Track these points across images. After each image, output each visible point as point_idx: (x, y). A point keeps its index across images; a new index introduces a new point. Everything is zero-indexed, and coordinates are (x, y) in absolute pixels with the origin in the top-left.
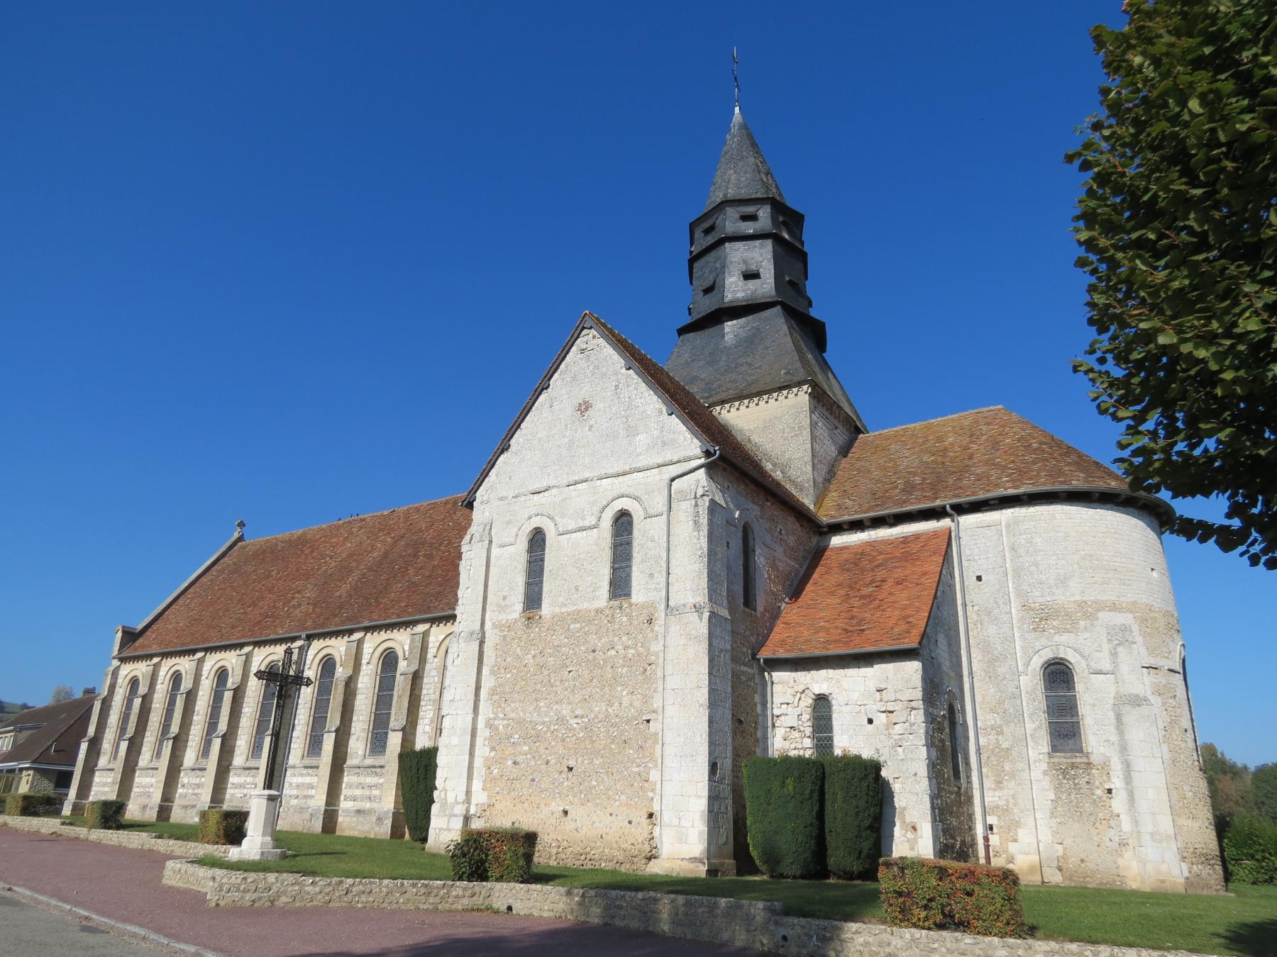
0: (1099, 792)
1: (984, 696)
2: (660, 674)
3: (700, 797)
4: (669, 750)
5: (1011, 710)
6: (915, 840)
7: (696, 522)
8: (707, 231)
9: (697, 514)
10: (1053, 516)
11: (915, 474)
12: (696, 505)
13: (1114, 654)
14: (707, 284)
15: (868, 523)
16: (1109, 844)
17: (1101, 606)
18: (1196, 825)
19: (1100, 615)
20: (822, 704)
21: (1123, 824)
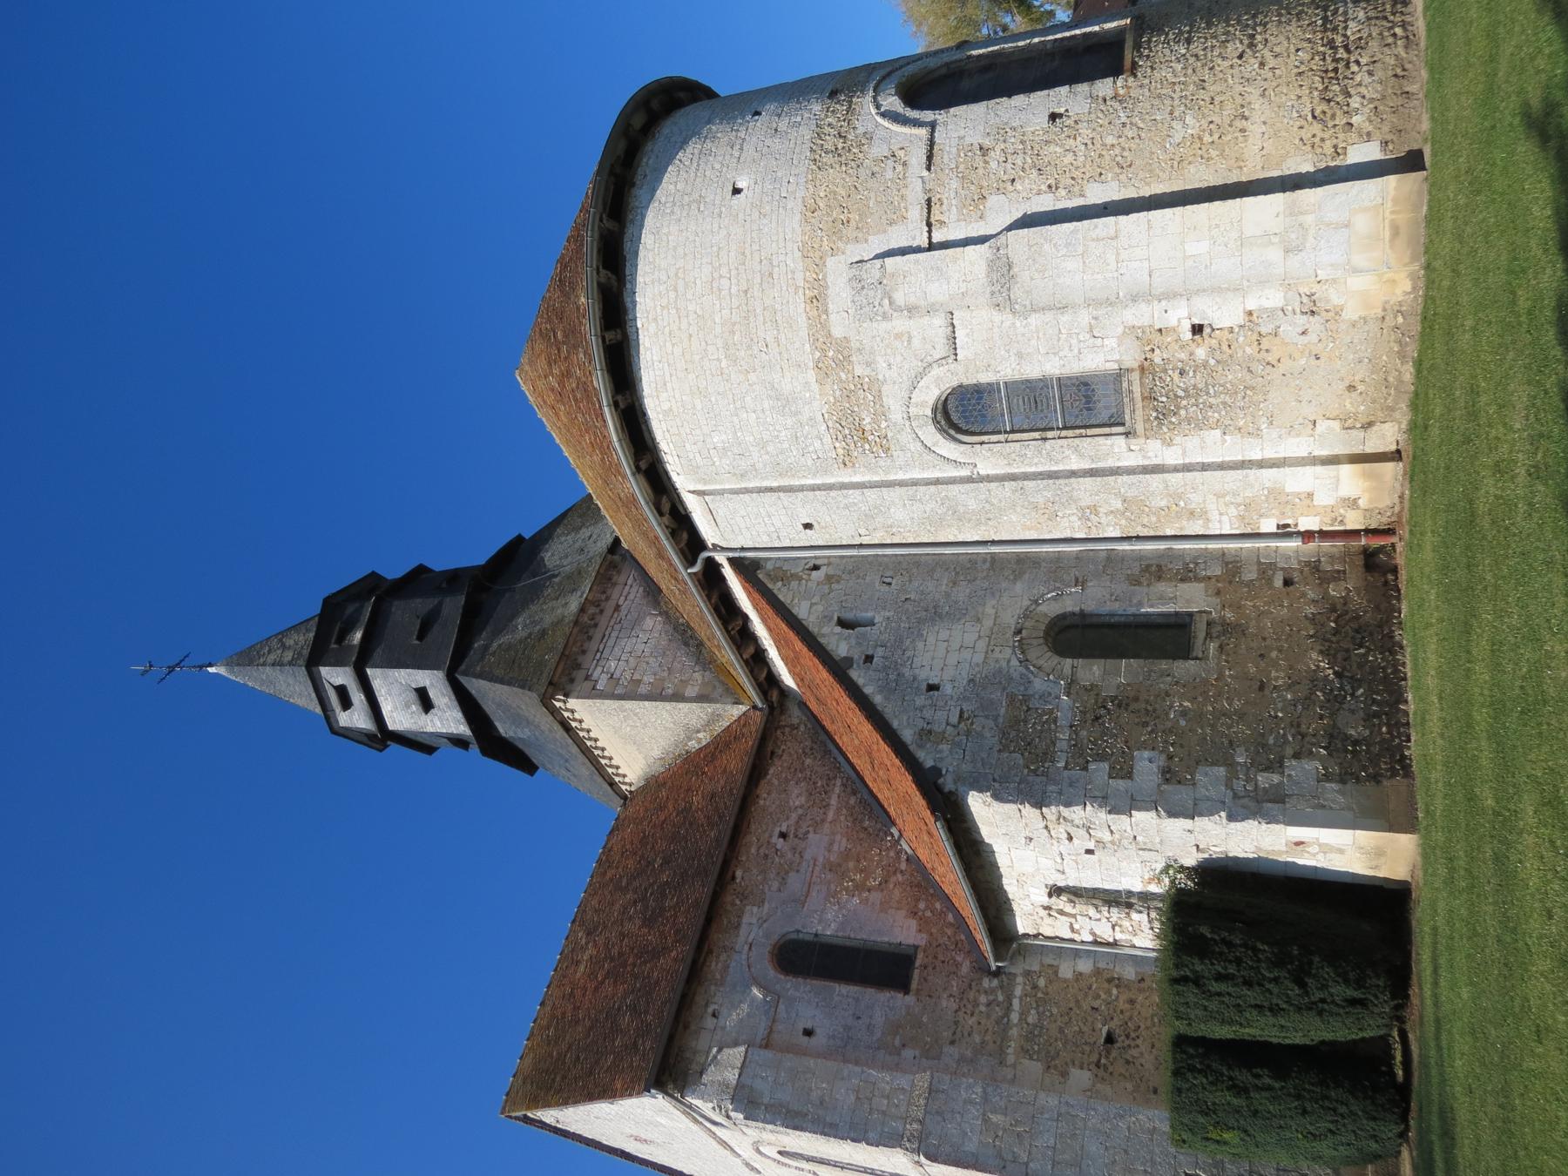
1: (1025, 528)
10: (667, 413)
13: (911, 310)
15: (610, 336)
16: (1312, 337)
17: (818, 1055)
18: (1259, 110)
19: (838, 332)
21: (1269, 304)
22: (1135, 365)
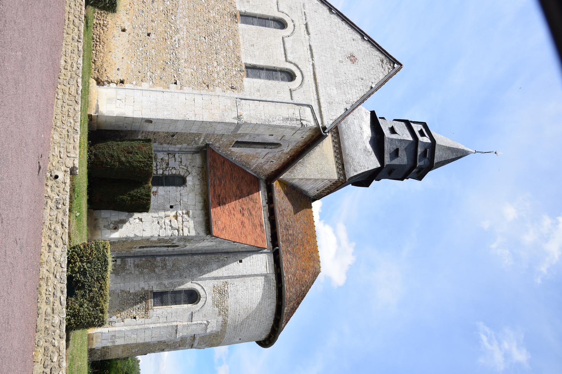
0: (134, 313)
2: (202, 92)
3: (133, 112)
4: (160, 95)
5: (174, 274)
6: (109, 229)
7: (287, 119)
8: (421, 132)
9: (292, 120)
11: (293, 231)
12: (297, 120)
14: (396, 129)
15: (271, 206)
20: (180, 181)
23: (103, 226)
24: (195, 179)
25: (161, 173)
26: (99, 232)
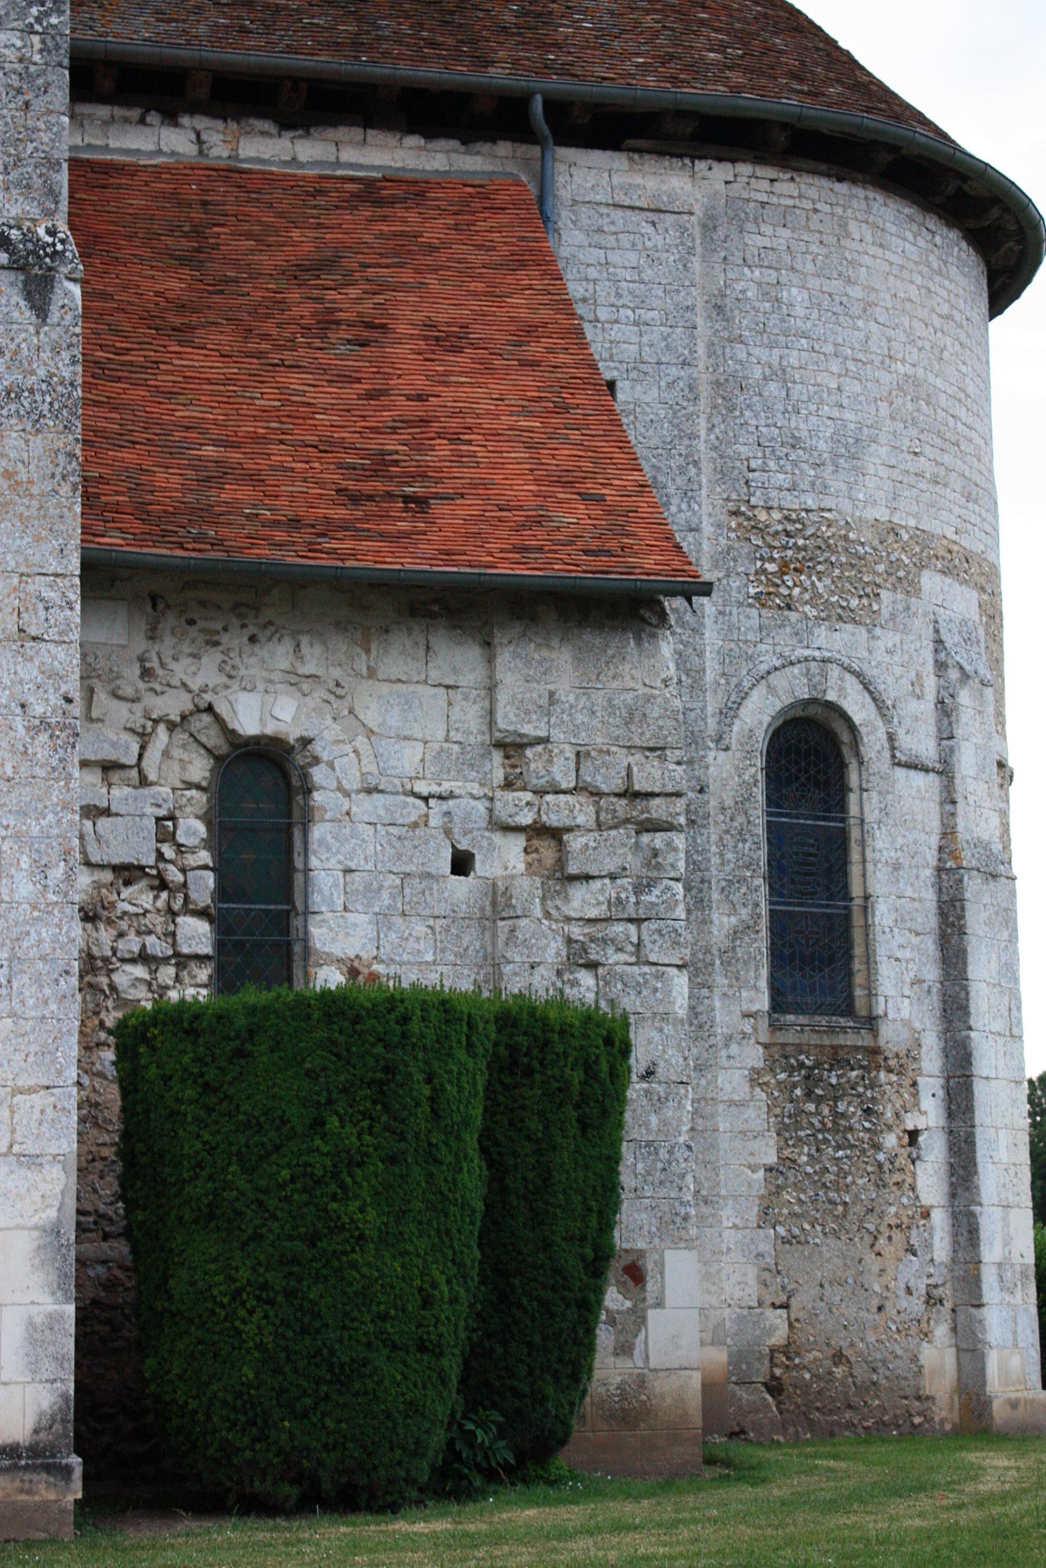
3: (32, 1161)
15: (781, 138)
22: (882, 1043)
23: (624, 1364)
24: (251, 666)
25: (203, 927)
26: (660, 1385)
